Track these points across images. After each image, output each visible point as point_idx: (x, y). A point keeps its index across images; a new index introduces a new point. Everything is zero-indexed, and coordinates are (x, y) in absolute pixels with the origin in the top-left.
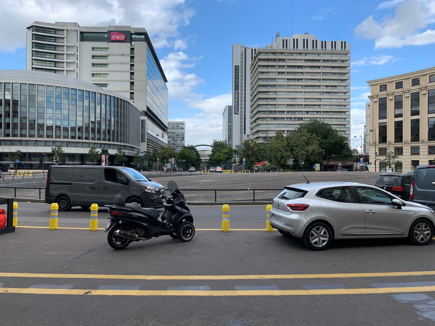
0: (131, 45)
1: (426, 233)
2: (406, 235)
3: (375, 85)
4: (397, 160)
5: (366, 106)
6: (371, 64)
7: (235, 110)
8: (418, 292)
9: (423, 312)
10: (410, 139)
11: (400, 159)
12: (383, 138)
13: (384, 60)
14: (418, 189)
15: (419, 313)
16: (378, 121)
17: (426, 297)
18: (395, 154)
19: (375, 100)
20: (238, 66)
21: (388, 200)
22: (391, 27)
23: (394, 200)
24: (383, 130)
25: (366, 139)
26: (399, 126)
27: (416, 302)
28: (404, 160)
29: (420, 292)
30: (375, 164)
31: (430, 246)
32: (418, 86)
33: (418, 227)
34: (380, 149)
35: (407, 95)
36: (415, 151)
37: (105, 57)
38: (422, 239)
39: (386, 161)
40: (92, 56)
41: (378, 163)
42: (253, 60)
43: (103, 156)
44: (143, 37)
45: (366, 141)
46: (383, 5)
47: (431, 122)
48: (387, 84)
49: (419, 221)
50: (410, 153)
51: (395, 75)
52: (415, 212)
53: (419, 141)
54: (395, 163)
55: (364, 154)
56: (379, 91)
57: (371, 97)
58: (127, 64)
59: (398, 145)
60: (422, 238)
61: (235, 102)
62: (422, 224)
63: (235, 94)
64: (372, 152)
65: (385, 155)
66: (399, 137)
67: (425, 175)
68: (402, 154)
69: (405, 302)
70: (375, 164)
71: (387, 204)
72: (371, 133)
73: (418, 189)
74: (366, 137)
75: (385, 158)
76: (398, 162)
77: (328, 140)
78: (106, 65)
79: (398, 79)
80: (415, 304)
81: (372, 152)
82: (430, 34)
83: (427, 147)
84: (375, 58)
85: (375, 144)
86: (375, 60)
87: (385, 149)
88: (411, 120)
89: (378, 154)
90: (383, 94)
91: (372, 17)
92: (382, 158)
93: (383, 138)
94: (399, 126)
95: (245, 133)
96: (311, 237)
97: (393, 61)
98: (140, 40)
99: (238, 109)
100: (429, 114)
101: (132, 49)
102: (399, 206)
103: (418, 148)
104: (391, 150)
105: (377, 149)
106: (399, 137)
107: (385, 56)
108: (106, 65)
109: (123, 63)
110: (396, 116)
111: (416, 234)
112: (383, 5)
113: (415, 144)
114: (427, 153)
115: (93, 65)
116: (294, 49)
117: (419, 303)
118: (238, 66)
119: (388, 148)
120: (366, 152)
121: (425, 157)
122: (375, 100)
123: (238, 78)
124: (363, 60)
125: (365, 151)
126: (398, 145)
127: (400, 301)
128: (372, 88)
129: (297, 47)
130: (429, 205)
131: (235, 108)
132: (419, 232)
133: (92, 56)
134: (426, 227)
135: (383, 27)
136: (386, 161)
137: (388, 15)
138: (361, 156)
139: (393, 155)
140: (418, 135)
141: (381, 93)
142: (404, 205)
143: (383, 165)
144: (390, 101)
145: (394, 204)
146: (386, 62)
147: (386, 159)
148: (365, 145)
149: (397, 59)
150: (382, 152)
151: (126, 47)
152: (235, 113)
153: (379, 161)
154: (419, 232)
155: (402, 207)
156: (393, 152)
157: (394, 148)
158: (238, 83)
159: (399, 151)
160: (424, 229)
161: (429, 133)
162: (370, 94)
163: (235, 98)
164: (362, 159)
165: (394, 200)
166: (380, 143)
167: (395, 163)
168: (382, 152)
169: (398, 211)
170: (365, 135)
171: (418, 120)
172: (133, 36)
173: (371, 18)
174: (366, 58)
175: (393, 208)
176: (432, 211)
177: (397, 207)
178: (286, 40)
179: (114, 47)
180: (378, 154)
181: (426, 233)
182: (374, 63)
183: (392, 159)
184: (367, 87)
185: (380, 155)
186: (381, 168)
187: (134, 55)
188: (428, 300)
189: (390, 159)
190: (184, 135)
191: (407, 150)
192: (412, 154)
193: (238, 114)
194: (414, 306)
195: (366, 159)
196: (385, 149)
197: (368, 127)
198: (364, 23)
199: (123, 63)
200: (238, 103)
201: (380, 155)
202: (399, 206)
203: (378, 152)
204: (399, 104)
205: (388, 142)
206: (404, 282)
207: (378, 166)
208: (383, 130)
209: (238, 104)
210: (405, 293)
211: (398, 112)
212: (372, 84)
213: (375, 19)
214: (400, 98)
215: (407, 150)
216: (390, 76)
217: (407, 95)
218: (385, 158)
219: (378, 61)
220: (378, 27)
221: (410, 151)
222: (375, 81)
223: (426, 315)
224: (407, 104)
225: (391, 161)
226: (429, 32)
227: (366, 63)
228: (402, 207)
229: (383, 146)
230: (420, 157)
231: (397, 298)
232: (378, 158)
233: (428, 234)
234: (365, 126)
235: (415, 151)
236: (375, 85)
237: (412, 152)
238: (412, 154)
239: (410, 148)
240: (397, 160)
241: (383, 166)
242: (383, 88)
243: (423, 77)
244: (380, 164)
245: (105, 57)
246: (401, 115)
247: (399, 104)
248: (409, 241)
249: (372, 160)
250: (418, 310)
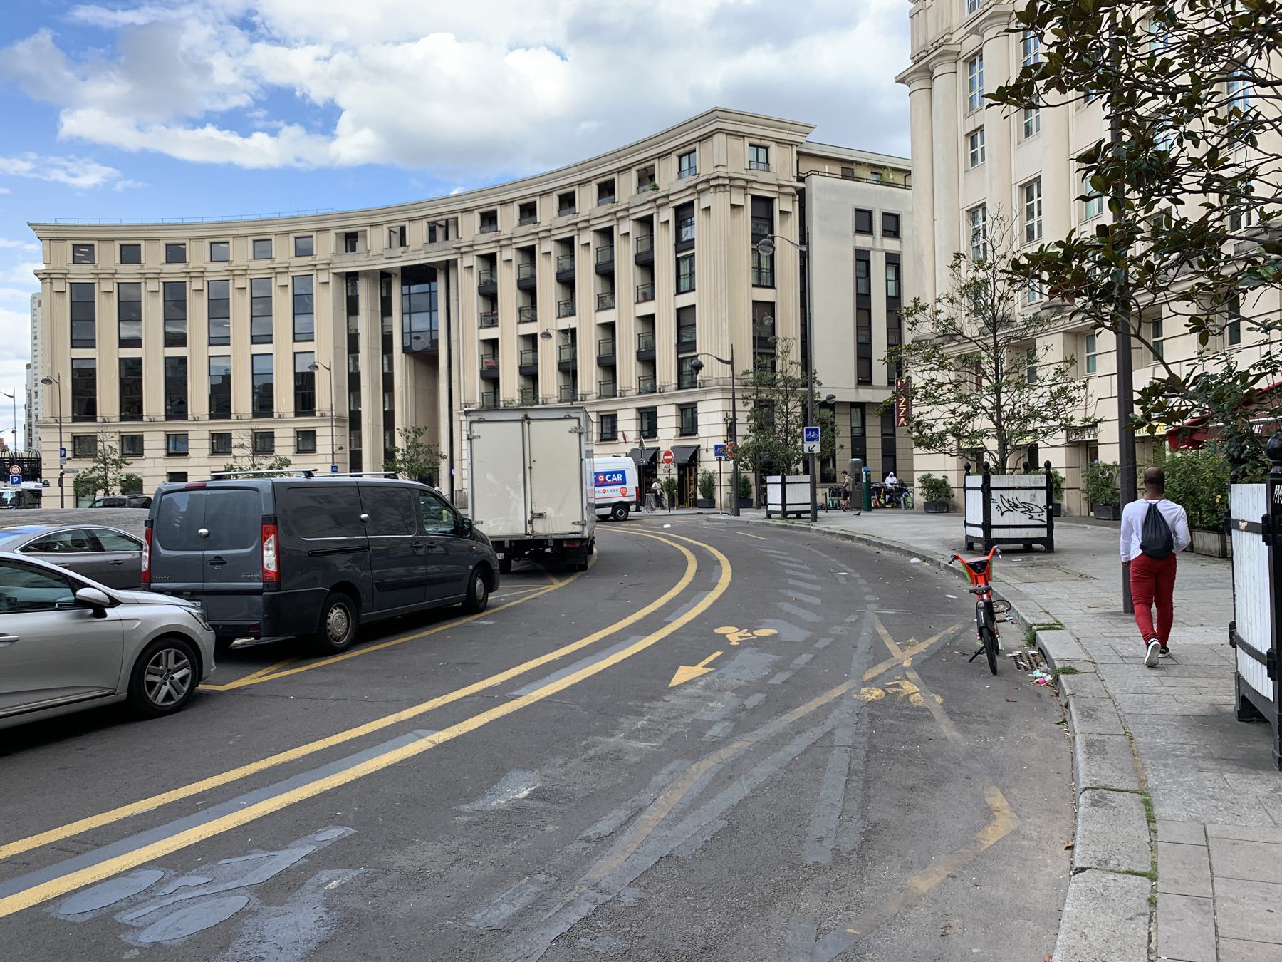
1: (177, 676)
2: (122, 693)
3: (58, 239)
4: (126, 470)
5: (32, 303)
6: (52, 178)
8: (135, 867)
9: (142, 928)
10: (163, 413)
11: (134, 468)
12: (85, 406)
13: (91, 176)
14: (163, 552)
15: (127, 938)
16: (67, 354)
17: (158, 874)
18: (123, 454)
19: (59, 286)
21: (64, 595)
22: (110, 87)
23: (82, 592)
24: (84, 382)
25: (34, 406)
26: (131, 374)
27: (124, 904)
28: (147, 472)
29: (117, 875)
30: (61, 485)
31: (189, 712)
32: (182, 265)
33: (157, 663)
34: (76, 439)
35: (153, 286)
36: (176, 445)
38: (168, 696)
39: (95, 474)
41: (69, 481)
45: (34, 413)
46: (86, 14)
47: (217, 368)
49: (159, 644)
50: (163, 453)
51: (118, 222)
52: (146, 621)
53: (186, 418)
54: (122, 482)
55: (26, 456)
56: (71, 260)
57: (44, 277)
59: (131, 428)
60: (168, 693)
62: (168, 653)
64: (50, 449)
65: (90, 456)
66: (131, 406)
67: (183, 509)
68: (142, 455)
69: (91, 915)
70: (61, 485)
71: (63, 606)
72: (47, 387)
73: (163, 552)
74: (34, 400)
75: (90, 465)
76: (129, 477)
77: (312, 479)
79: (130, 237)
80: (122, 909)
81: (50, 449)
82: (211, 138)
83: (207, 435)
84: (65, 163)
85: (59, 422)
86: (65, 168)
87: (93, 440)
89: (69, 455)
90: (82, 273)
91: (49, 37)
92: (84, 466)
93: (85, 406)
94: (131, 374)
96: (150, 690)
97: (119, 187)
100: (210, 345)
102: (98, 609)
104: (109, 441)
105: (67, 438)
106: (131, 406)
107: (95, 166)
110: (123, 343)
111: (152, 685)
112: (86, 14)
113: (176, 427)
114: (207, 452)
117: (132, 902)
119: (100, 437)
120: (34, 447)
122: (59, 286)
124: (25, 160)
125: (30, 445)
126: (131, 428)
127: (70, 919)
128: (47, 249)
130: (191, 595)
132: (157, 679)
134: (178, 659)
135: (84, 79)
136: (95, 474)
137: (102, 51)
138: (14, 460)
139: (116, 457)
140: (183, 403)
141: (76, 268)
142: (114, 603)
143: (84, 487)
144: (103, 296)
145: (82, 604)
146: (96, 185)
147: (94, 469)
148: (30, 425)
149: (130, 182)
150: (84, 447)
153: (73, 476)
154: (157, 679)
155: (108, 611)
156: (117, 447)
157: (117, 437)
159: (133, 446)
160: (172, 665)
161: (210, 397)
162: (42, 267)
164: (15, 470)
165: (82, 592)
166: (74, 419)
167: (122, 482)
168: (84, 447)
169: (97, 625)
170: (29, 396)
171: (183, 361)
173: (45, 37)
174: (33, 156)
175: (81, 616)
176: (195, 612)
177: (91, 611)
180: (69, 455)
181: (177, 676)
182: (60, 176)
183: (112, 468)
184: (36, 247)
185: (75, 456)
186: (78, 496)
188: (160, 883)
189: (106, 470)
191: (154, 443)
192: (169, 454)
194: (118, 917)
195: (32, 470)
196: (93, 440)
197: (39, 371)
198: (22, 48)
201: (75, 456)
202: (98, 609)
203: (68, 447)
204: (129, 310)
205: (99, 419)
206: (98, 846)
207: (69, 491)
208: (84, 382)
210: (76, 891)
211: (129, 331)
212: (48, 234)
213: (60, 44)
214: (132, 291)
215: (154, 443)
216: (103, 222)
217: (153, 286)
218: (90, 465)
219: (73, 175)
220: (68, 75)
221: (162, 445)
222: (57, 227)
223: (146, 937)
224: (153, 309)
225: (110, 474)
226: (210, 131)
227: (34, 171)
228: (108, 611)
229: (84, 428)
230: (191, 462)
231: (64, 911)
232: (68, 465)
233: (183, 680)
234: (29, 366)
235: (176, 445)
236: (58, 239)
237: (167, 449)
238: (169, 454)
239: (162, 436)
240: (126, 470)
241: (87, 492)
242: (83, 253)
244: (77, 484)
246: (136, 343)
247: (129, 310)
248: (131, 708)
249: (49, 471)
250: (128, 928)
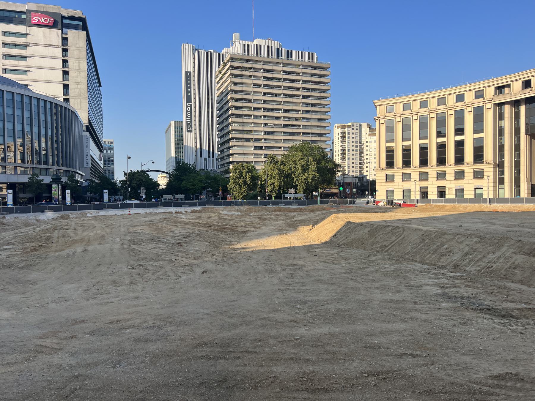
0: (62, 33)
3: (382, 105)
7: (187, 126)
12: (390, 164)
20: (190, 72)
28: (466, 185)
37: (24, 46)
40: (3, 43)
42: (221, 67)
43: (54, 186)
44: (80, 23)
48: (395, 104)
58: (58, 58)
61: (187, 117)
63: (187, 107)
78: (24, 58)
88: (437, 143)
93: (390, 164)
95: (201, 156)
98: (75, 27)
99: (191, 126)
101: (65, 40)
103: (445, 174)
108: (24, 58)
109: (51, 57)
115: (5, 56)
116: (268, 57)
118: (190, 72)
121: (471, 182)
123: (190, 88)
129: (260, 54)
131: (187, 124)
133: (3, 43)
141: (388, 114)
151: (55, 35)
152: (188, 131)
158: (191, 94)
163: (187, 111)
172: (65, 21)
178: (248, 45)
179: (38, 34)
187: (68, 48)
190: (113, 157)
193: (191, 132)
199: (51, 57)
200: (191, 118)
208: (390, 153)
209: (191, 120)
230: (429, 183)
236: (382, 105)
243: (431, 99)
245: (24, 46)
